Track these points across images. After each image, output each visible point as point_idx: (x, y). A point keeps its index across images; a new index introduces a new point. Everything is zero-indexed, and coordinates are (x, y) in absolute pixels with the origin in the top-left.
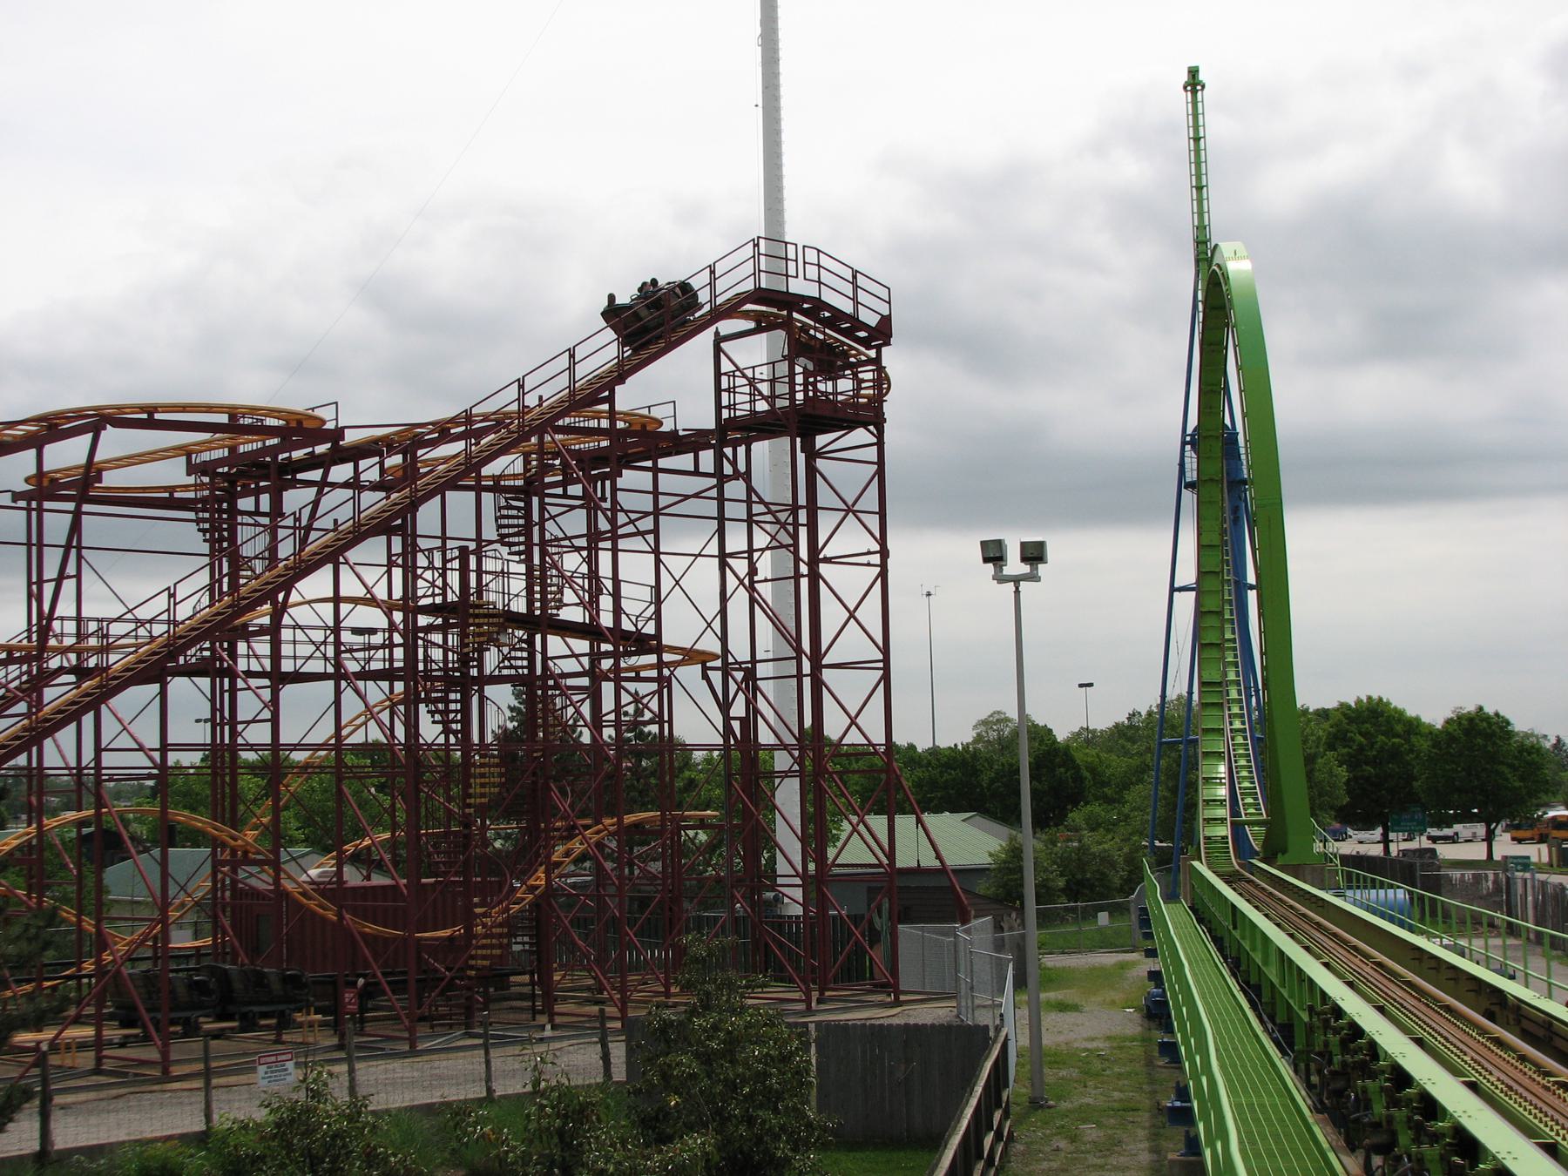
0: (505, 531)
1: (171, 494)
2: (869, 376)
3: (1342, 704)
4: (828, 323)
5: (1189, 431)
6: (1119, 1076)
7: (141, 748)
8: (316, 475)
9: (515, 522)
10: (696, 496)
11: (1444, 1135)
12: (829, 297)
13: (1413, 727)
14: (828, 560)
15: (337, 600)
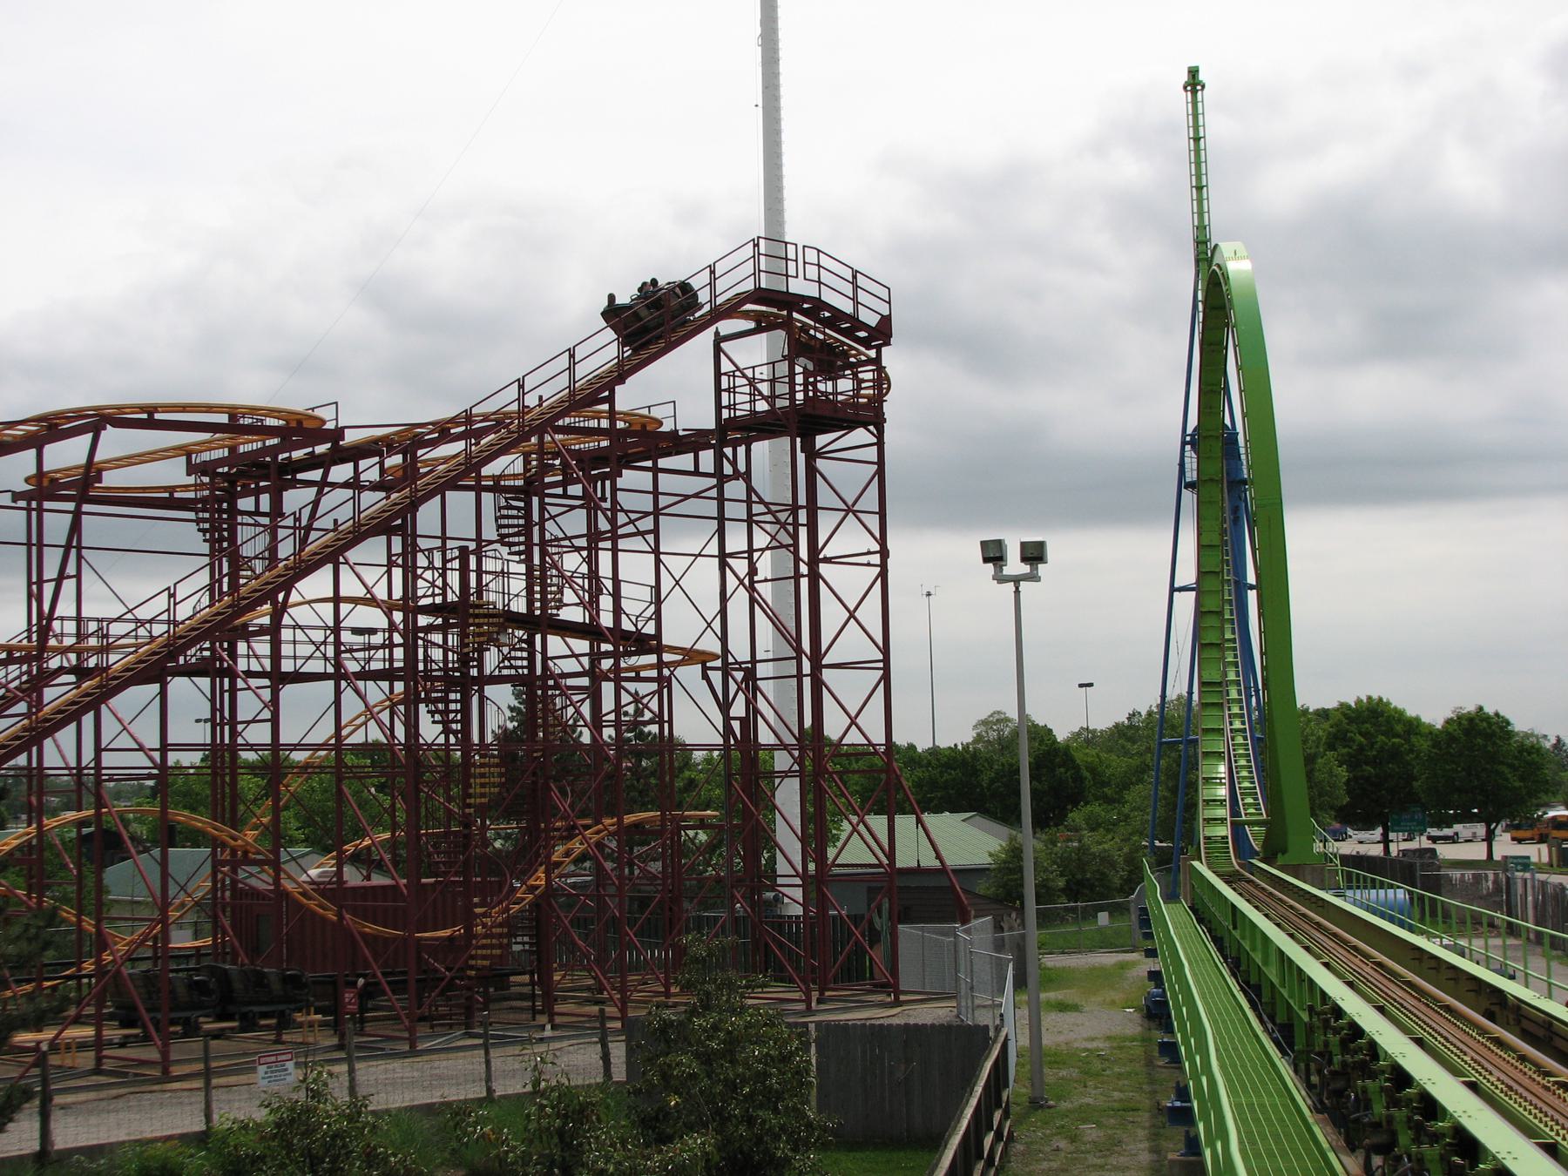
0: (505, 531)
1: (171, 494)
2: (869, 376)
3: (1342, 704)
4: (828, 323)
5: (1189, 431)
6: (1119, 1076)
7: (141, 748)
8: (316, 475)
9: (515, 522)
10: (696, 496)
11: (1444, 1135)
12: (829, 297)
13: (1413, 727)
14: (828, 560)
15: (337, 600)
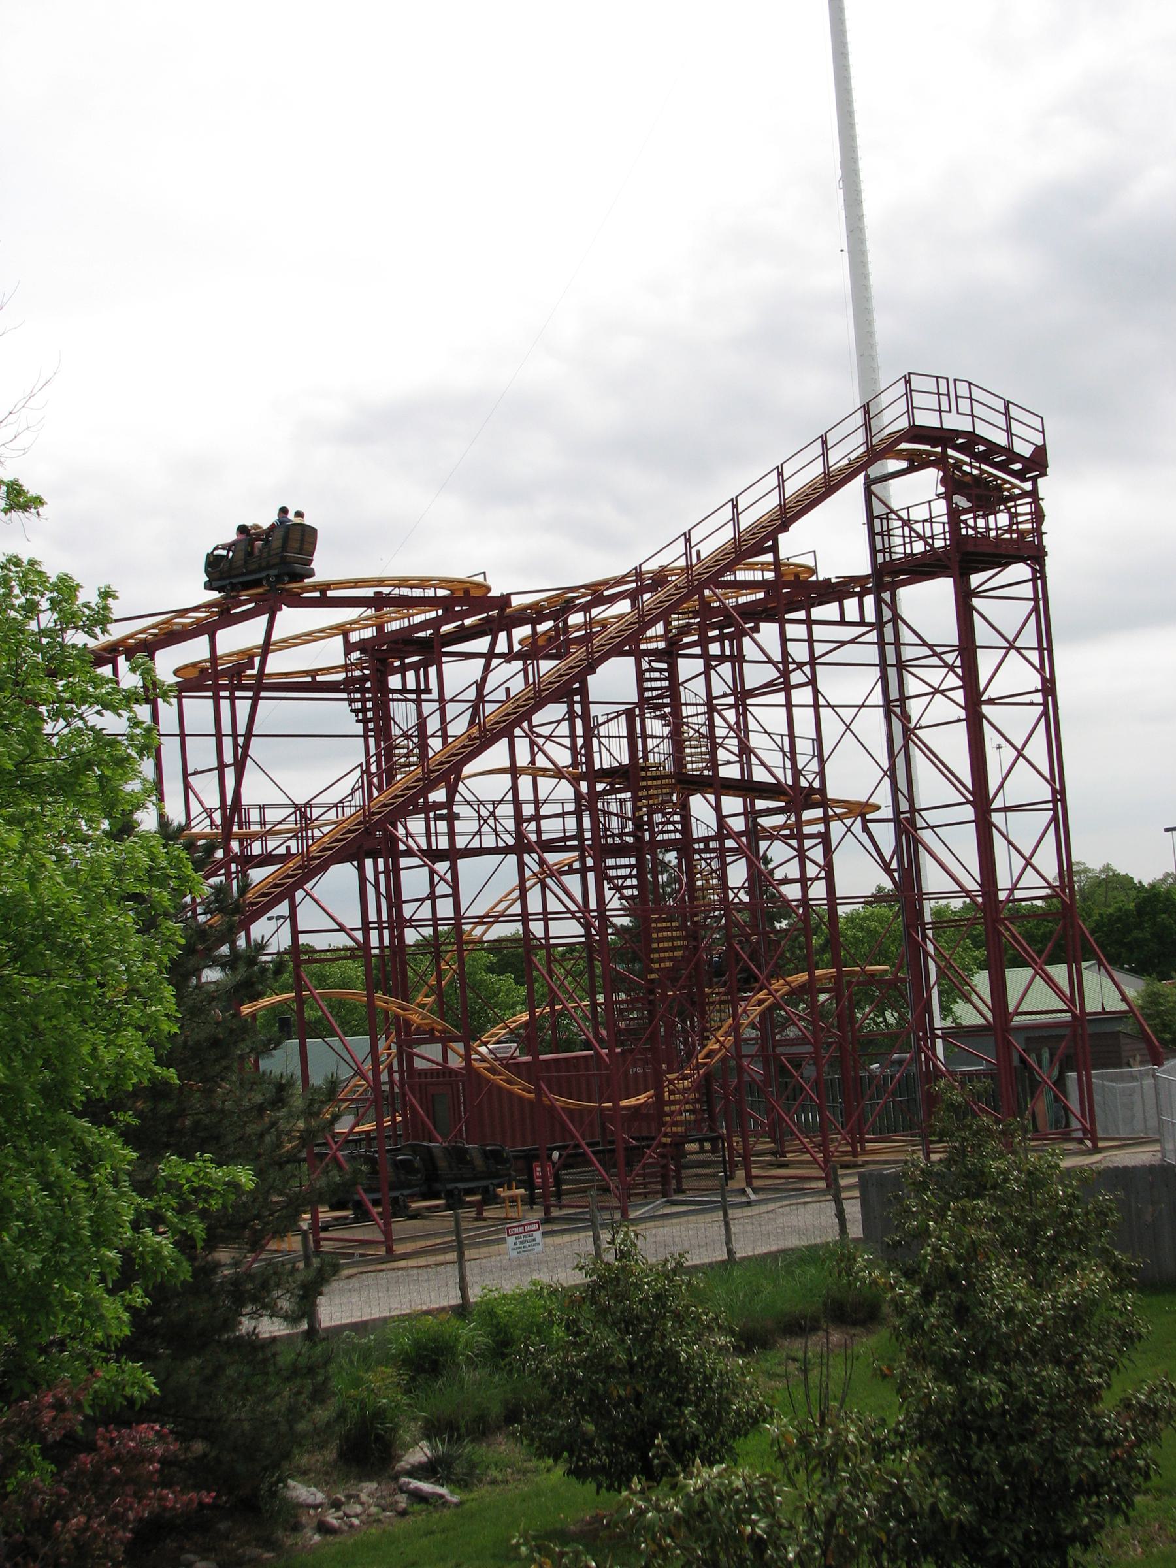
1: (313, 678)
2: (1027, 509)
4: (983, 458)
7: (342, 928)
8: (481, 644)
9: (658, 684)
10: (843, 643)
12: (983, 430)
14: (991, 701)
15: (514, 771)
